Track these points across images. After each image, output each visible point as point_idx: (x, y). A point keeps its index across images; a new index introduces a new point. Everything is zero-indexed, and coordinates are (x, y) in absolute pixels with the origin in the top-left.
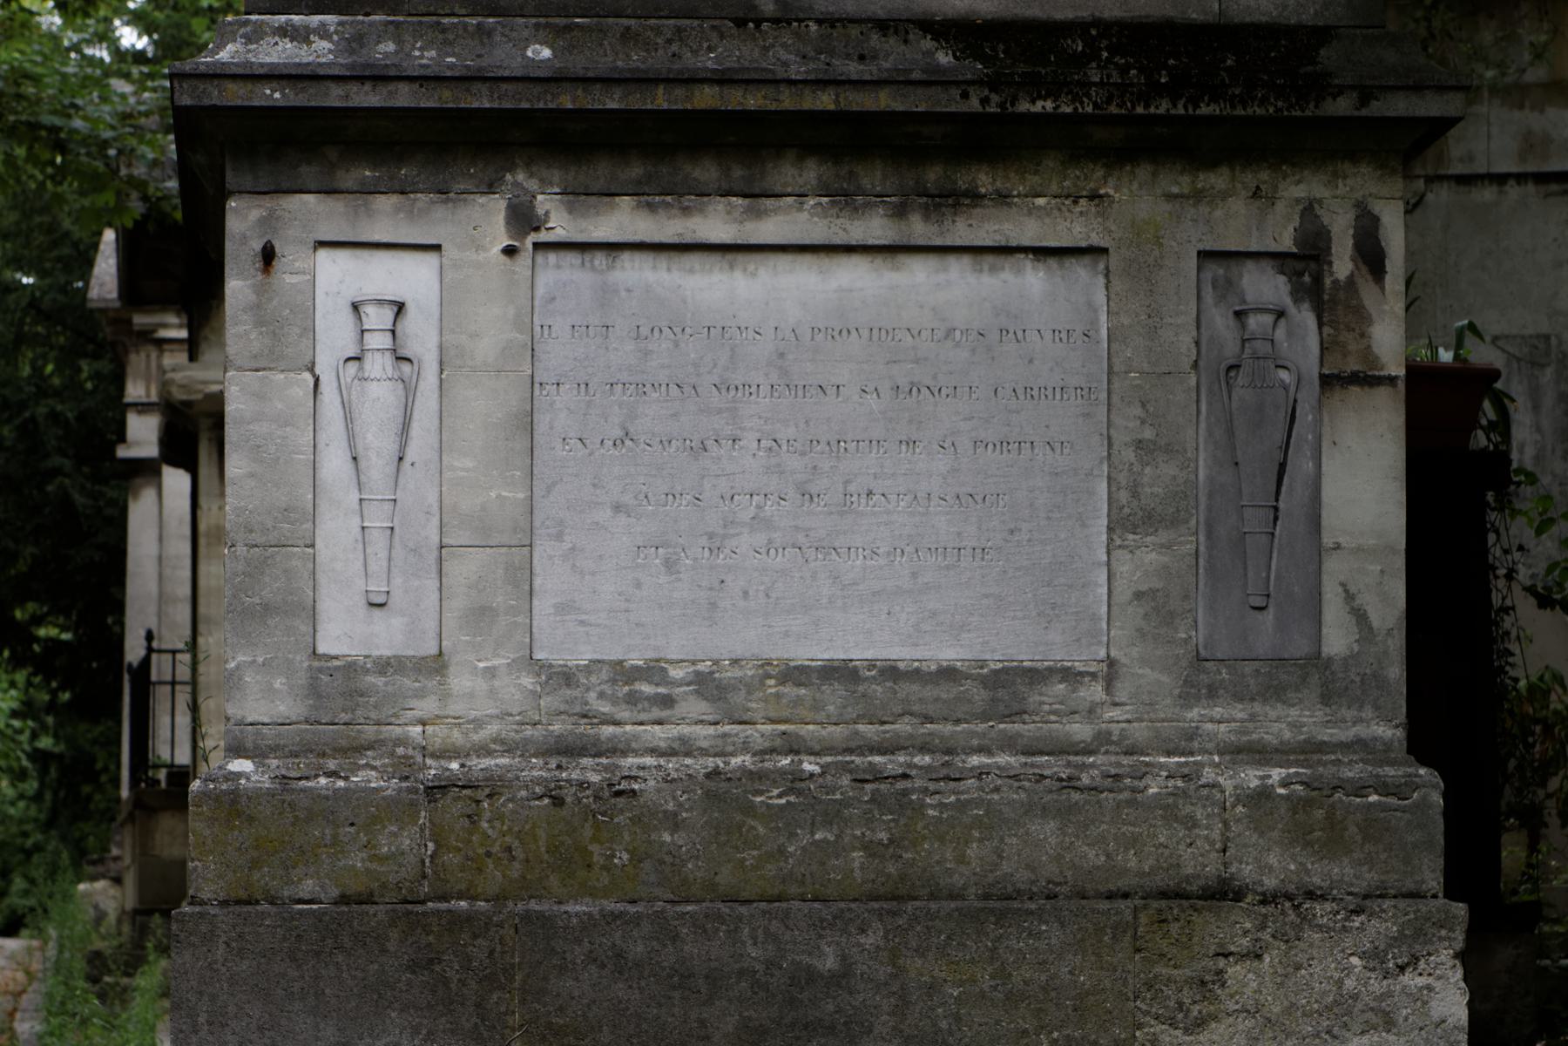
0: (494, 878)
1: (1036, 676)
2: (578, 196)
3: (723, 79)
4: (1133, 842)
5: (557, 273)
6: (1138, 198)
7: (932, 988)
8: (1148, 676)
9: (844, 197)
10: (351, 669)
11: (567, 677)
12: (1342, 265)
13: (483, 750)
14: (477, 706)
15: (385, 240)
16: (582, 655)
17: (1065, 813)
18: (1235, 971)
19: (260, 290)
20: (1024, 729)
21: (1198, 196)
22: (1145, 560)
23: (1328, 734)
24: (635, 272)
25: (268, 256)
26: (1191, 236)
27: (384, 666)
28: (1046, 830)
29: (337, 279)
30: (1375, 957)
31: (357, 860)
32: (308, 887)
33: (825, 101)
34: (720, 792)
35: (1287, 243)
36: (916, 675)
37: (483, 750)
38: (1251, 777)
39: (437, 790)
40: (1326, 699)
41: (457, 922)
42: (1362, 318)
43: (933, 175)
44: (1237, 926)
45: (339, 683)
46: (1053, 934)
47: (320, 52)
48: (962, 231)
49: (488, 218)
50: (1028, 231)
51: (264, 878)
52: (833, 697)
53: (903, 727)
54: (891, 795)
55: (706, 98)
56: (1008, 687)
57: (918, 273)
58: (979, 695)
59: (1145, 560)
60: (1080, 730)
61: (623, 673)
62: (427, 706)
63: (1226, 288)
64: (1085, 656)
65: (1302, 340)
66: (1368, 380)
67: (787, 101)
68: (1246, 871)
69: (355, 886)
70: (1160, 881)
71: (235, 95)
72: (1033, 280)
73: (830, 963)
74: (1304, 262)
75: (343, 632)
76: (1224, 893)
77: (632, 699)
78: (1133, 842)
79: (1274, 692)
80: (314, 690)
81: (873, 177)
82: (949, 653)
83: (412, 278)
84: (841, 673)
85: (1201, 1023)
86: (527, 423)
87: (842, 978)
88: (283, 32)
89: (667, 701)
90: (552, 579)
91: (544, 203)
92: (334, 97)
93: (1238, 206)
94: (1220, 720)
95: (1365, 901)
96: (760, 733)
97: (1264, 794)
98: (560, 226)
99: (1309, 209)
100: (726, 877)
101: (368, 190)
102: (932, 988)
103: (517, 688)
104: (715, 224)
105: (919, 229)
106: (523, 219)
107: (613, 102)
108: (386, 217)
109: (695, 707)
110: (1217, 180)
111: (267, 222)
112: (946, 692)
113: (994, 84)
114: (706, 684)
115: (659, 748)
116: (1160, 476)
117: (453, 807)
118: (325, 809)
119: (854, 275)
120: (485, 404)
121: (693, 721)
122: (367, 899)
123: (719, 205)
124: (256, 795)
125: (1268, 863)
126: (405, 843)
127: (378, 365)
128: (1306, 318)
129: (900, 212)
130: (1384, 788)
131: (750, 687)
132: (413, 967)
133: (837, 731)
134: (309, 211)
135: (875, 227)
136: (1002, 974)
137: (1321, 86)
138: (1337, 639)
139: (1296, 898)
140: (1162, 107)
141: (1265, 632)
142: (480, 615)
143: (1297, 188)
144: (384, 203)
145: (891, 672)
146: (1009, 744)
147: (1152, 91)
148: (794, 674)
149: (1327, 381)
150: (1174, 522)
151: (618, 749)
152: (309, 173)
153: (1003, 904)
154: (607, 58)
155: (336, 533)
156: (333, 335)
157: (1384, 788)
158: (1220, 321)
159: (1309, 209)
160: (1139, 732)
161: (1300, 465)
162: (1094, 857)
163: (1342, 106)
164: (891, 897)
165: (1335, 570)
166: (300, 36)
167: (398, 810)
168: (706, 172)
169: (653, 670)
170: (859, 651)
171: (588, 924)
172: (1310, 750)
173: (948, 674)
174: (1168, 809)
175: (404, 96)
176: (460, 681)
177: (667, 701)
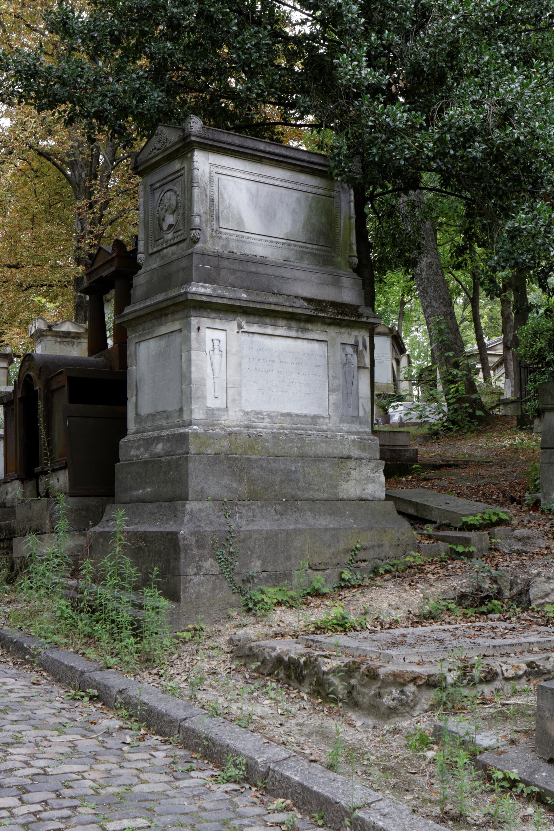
0: (240, 451)
1: (318, 417)
2: (248, 322)
3: (276, 304)
4: (336, 448)
5: (245, 337)
6: (332, 332)
7: (309, 474)
8: (335, 418)
9: (289, 327)
10: (213, 410)
11: (247, 413)
12: (361, 347)
13: (234, 426)
14: (233, 418)
15: (375, 355)
16: (249, 409)
17: (327, 442)
18: (352, 472)
19: (198, 335)
20: (317, 427)
21: (340, 333)
22: (334, 398)
23: (360, 430)
24: (257, 338)
25: (199, 329)
26: (340, 340)
27: (218, 409)
28: (323, 445)
29: (209, 335)
30: (372, 470)
31: (217, 446)
32: (209, 451)
33: (290, 310)
34: (275, 436)
35: (353, 343)
36: (301, 416)
37: (234, 426)
38: (352, 437)
39: (230, 434)
40: (360, 423)
41: (236, 459)
42: (363, 356)
43: (302, 325)
44: (352, 464)
45: (210, 412)
46: (327, 465)
47: (209, 291)
48: (307, 335)
49: (232, 326)
50: (316, 337)
51: (202, 450)
52: (289, 419)
53: (299, 425)
54: (301, 438)
55: (273, 307)
56: (315, 419)
57: (299, 342)
58: (310, 420)
59: (334, 398)
60: (325, 428)
61: (257, 413)
62: (225, 418)
63: (344, 349)
64: (325, 414)
65: (354, 359)
66: (364, 368)
67: (285, 309)
68: (352, 454)
69: (217, 452)
70: (340, 455)
71: (198, 298)
72: (316, 345)
73: (293, 469)
74: (355, 346)
75: (211, 403)
76: (349, 458)
77: (258, 418)
78: (336, 448)
79: (353, 422)
80: (207, 413)
81: (293, 324)
82: (305, 412)
83: (221, 335)
84: (289, 415)
85: (348, 481)
86: (240, 365)
87: (296, 471)
88: (202, 286)
89: (263, 419)
90: (244, 394)
91: (243, 324)
92: (214, 300)
93: (346, 335)
94: (345, 427)
95: (370, 460)
96: (277, 425)
97: (354, 440)
98: (246, 328)
99: (356, 337)
100: (276, 452)
101: (214, 318)
102: (309, 474)
103: (240, 415)
104: (269, 330)
105: (300, 335)
106: (240, 327)
107: (258, 306)
108: (218, 324)
109: (267, 420)
110: (343, 330)
111: (198, 322)
112: (305, 419)
113: (316, 310)
114: (269, 416)
115: (264, 427)
116: (336, 382)
117: (233, 437)
118: (211, 437)
119: (290, 342)
120: (233, 360)
121: (267, 423)
122: (219, 454)
123: (270, 327)
124: (201, 433)
125: (355, 453)
126: (225, 443)
127: (217, 351)
128: (355, 356)
129: (297, 331)
130: (371, 440)
131: (276, 417)
132: (229, 467)
133: (289, 426)
134: (205, 322)
135: (293, 334)
136: (319, 471)
137: (361, 316)
138: (361, 414)
139: (360, 459)
140: (339, 317)
141: (351, 411)
142: (234, 400)
143: (355, 333)
144: (218, 321)
145: (297, 415)
146: (315, 429)
147: (338, 314)
148: (283, 415)
149: (358, 367)
150: (338, 391)
151: (255, 427)
152: (205, 314)
153: (318, 459)
154: (255, 298)
155: (209, 383)
156: (209, 346)
157: (371, 440)
158: (344, 356)
159: (356, 337)
160: (334, 428)
161: (355, 382)
162: (330, 450)
163: (364, 320)
164: (302, 457)
165: (361, 400)
166: (205, 287)
167: (224, 437)
168: (268, 320)
169: (261, 413)
170: (292, 411)
171: (257, 460)
172: (358, 433)
173: (306, 416)
174: (341, 442)
175: (225, 301)
176: (231, 413)
177: (263, 419)
